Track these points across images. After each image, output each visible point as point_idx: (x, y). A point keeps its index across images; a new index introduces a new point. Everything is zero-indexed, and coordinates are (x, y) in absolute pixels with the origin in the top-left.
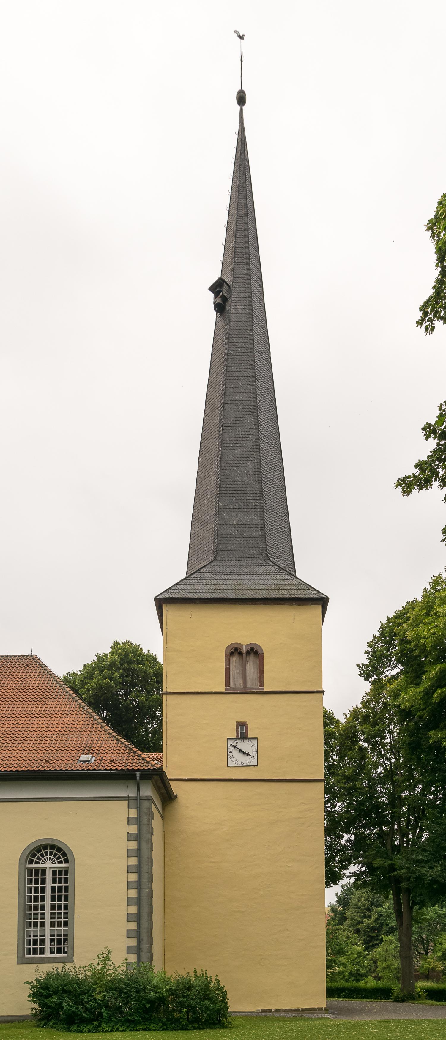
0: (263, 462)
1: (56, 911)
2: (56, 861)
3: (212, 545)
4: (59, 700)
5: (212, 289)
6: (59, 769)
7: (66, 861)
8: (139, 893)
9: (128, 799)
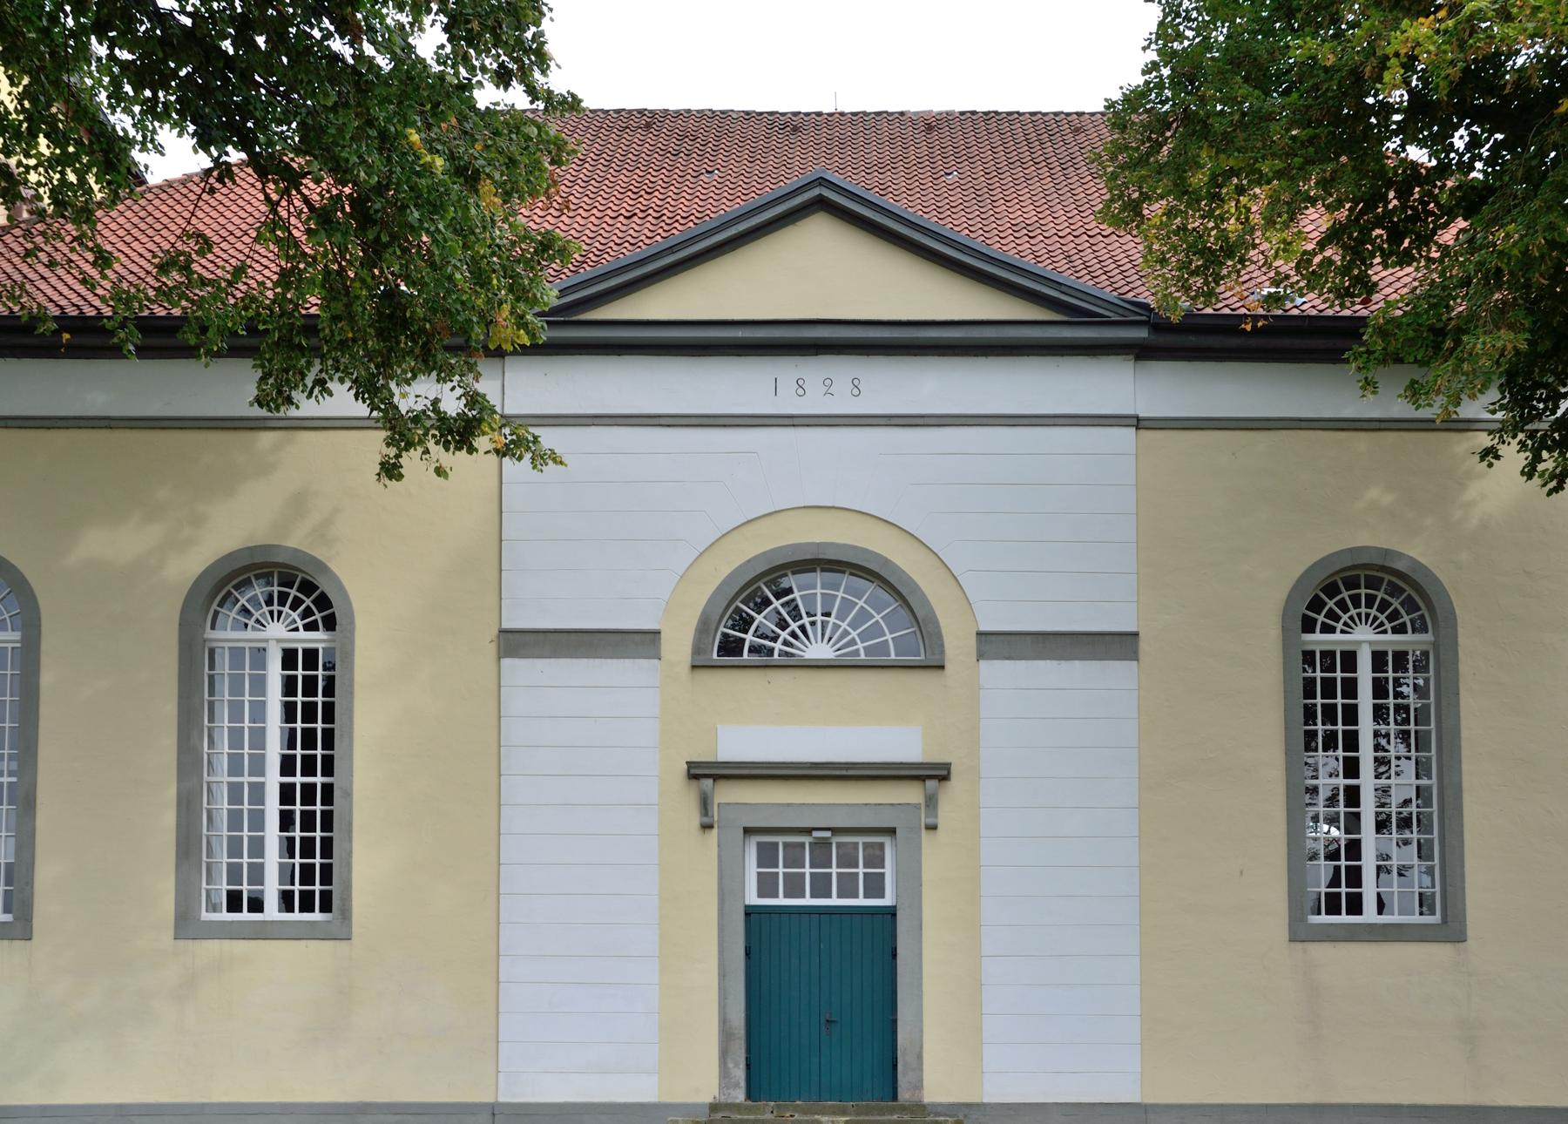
2: (1388, 626)
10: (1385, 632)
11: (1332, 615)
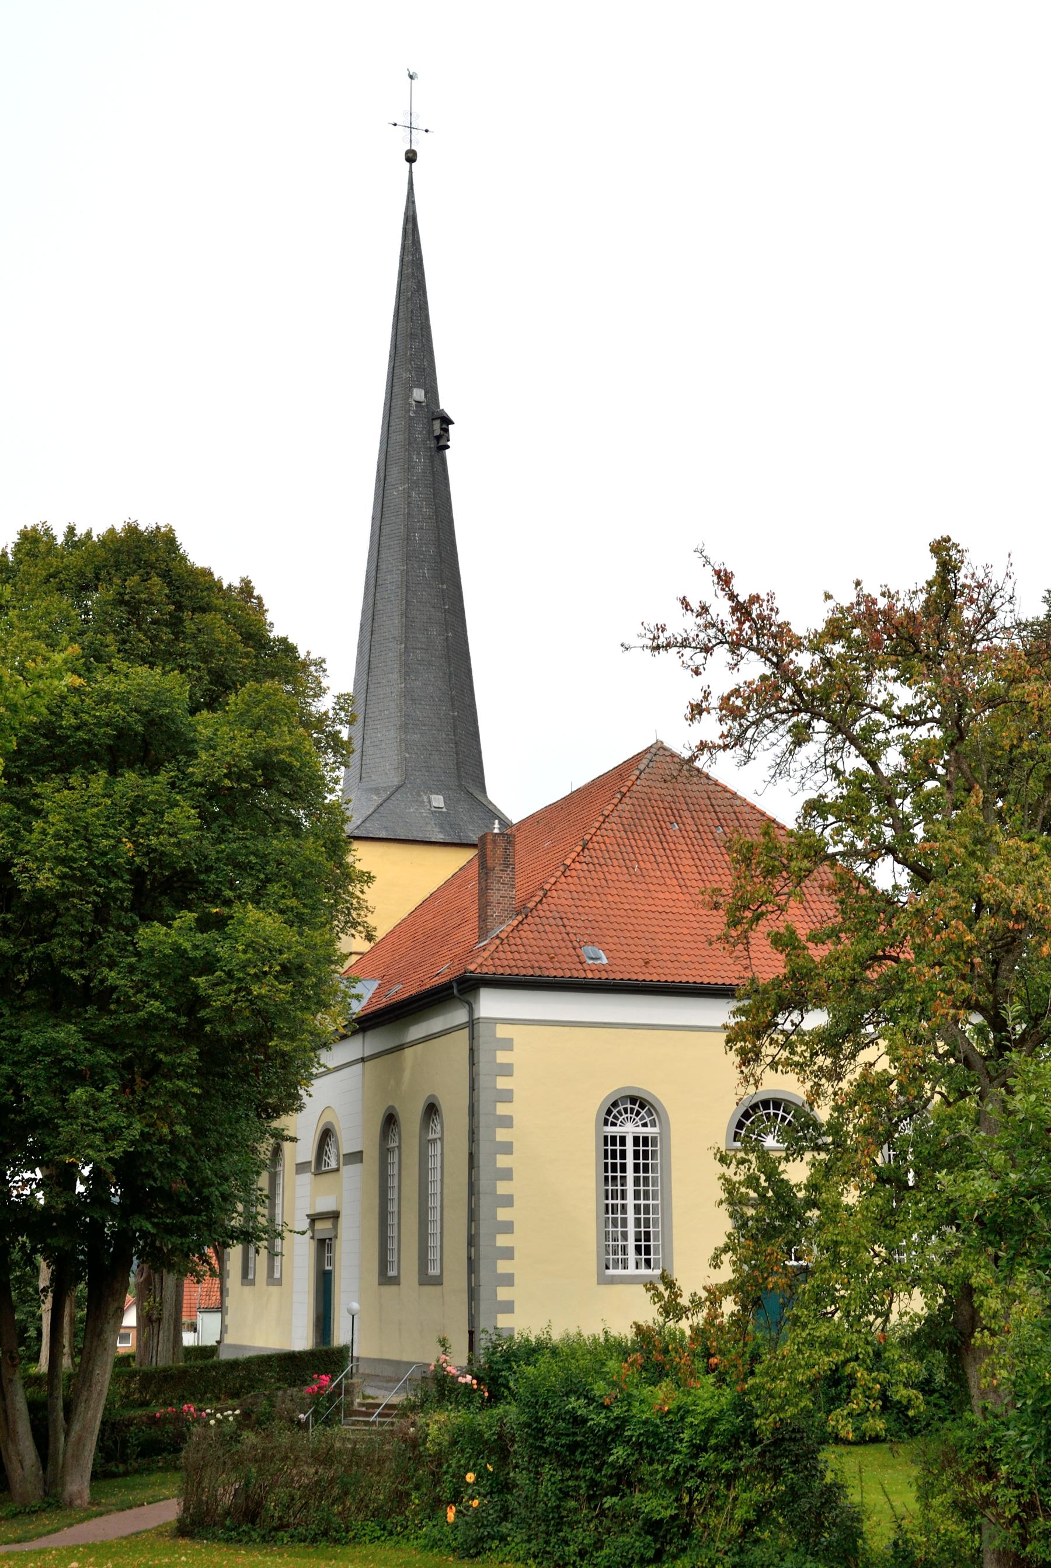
11: (615, 1117)
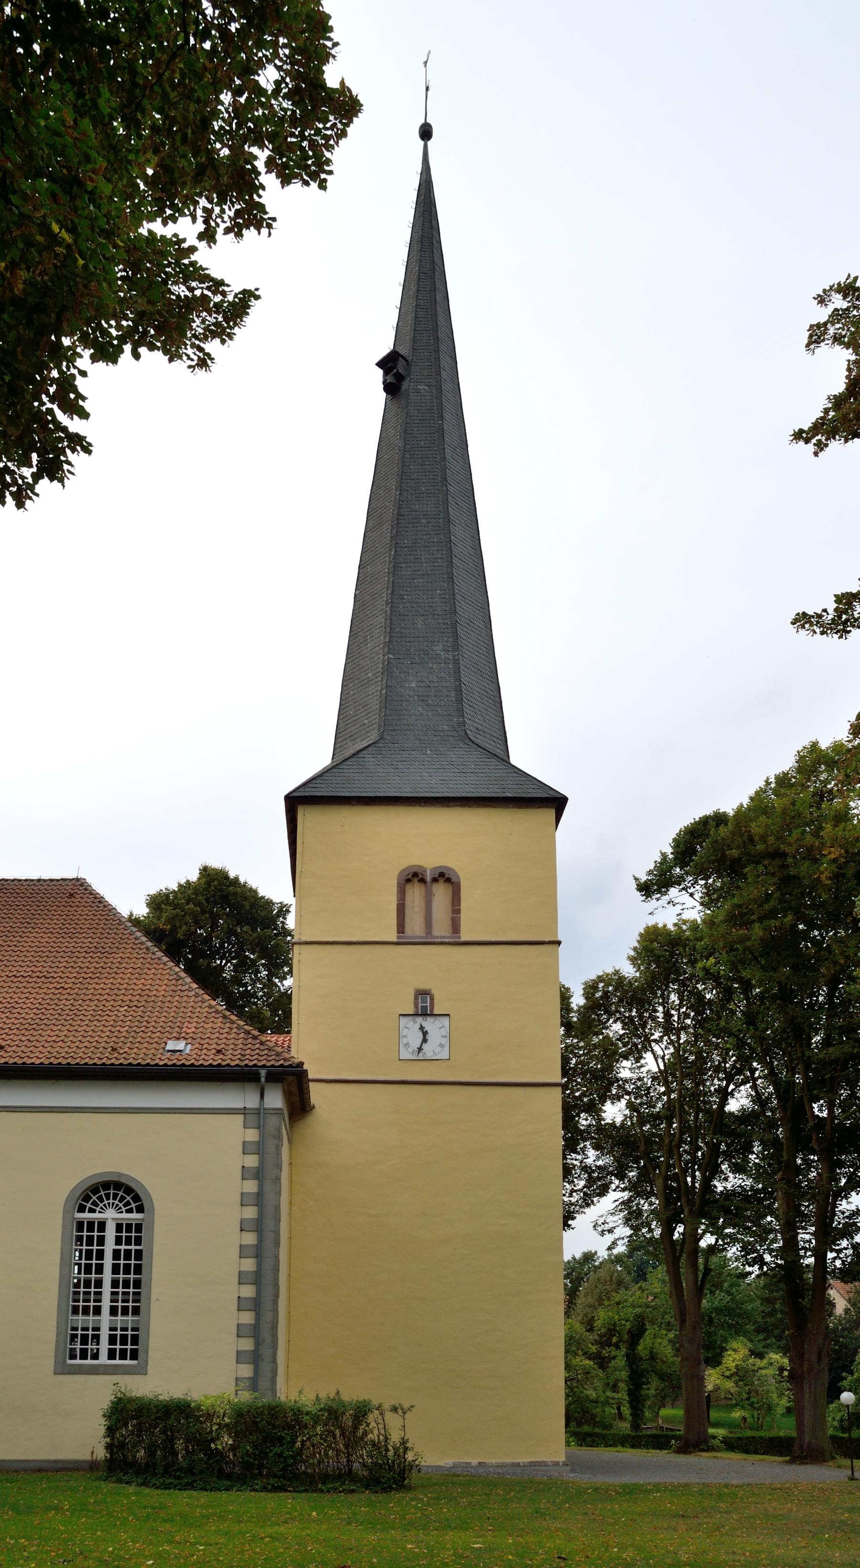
0: (458, 597)
1: (121, 1290)
2: (124, 1209)
3: (377, 716)
4: (126, 951)
5: (381, 364)
6: (135, 1062)
7: (140, 1209)
8: (259, 1265)
9: (244, 1111)
10: (122, 1212)
